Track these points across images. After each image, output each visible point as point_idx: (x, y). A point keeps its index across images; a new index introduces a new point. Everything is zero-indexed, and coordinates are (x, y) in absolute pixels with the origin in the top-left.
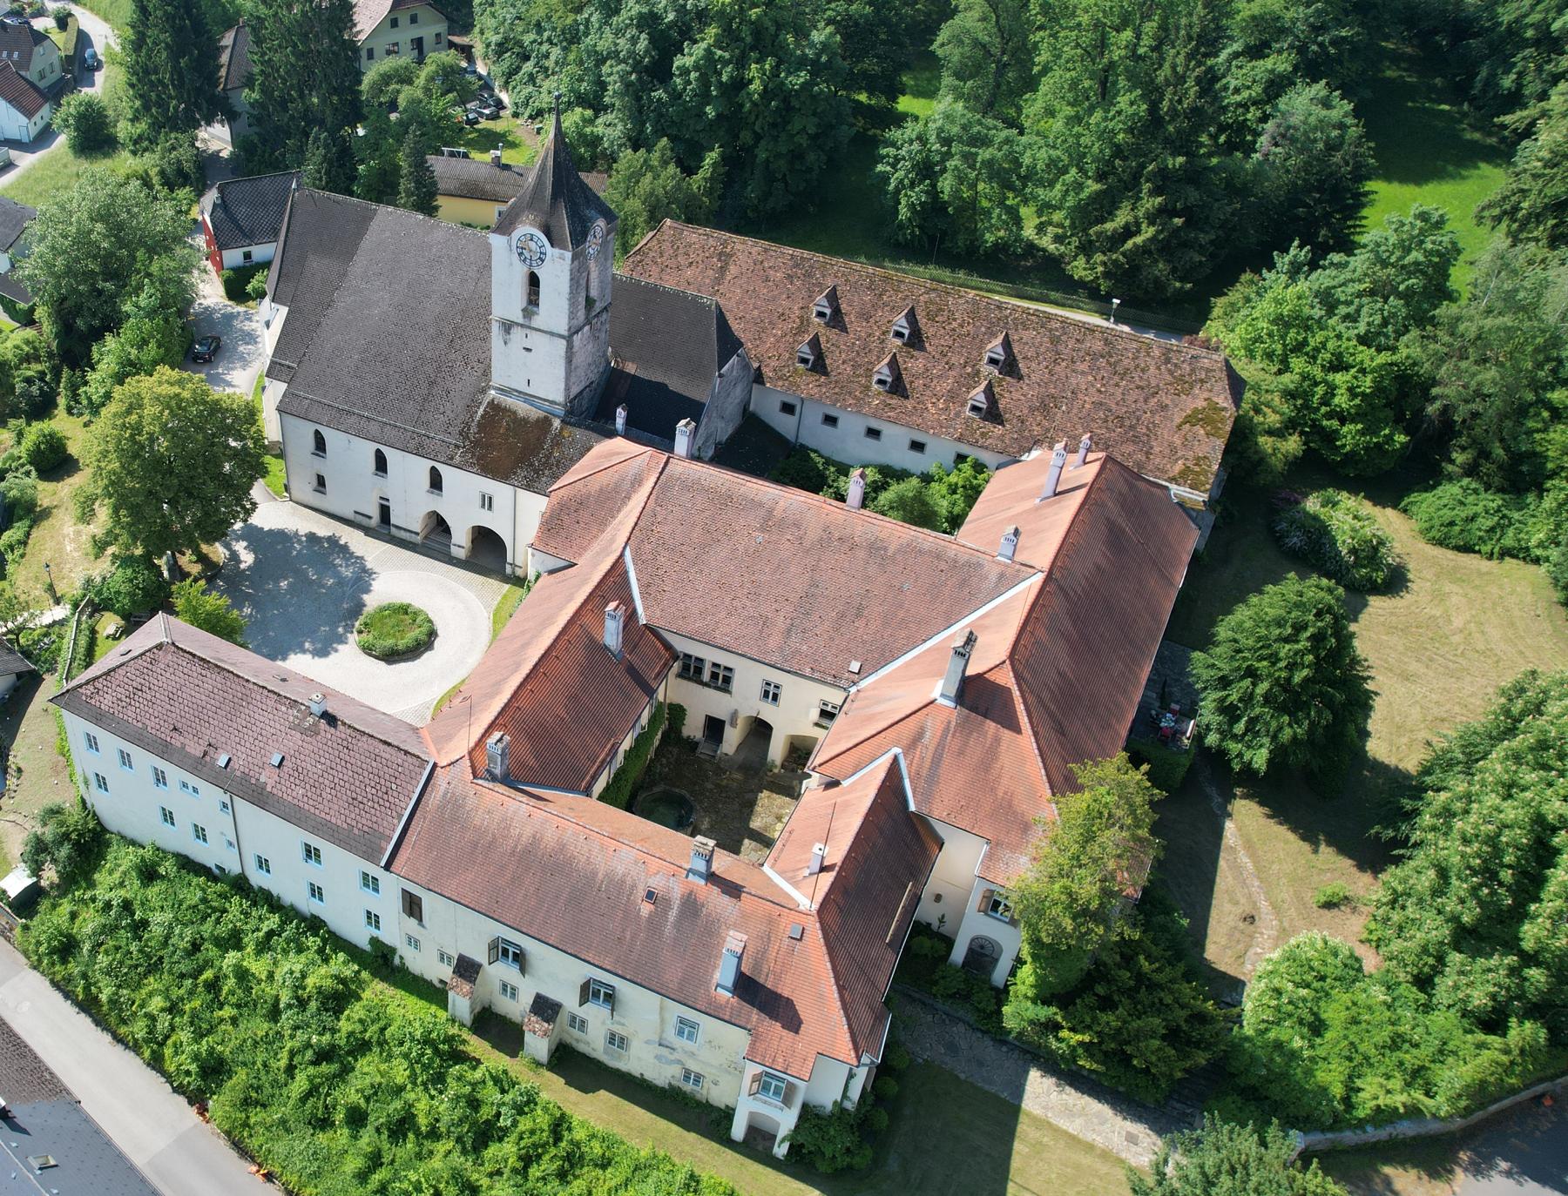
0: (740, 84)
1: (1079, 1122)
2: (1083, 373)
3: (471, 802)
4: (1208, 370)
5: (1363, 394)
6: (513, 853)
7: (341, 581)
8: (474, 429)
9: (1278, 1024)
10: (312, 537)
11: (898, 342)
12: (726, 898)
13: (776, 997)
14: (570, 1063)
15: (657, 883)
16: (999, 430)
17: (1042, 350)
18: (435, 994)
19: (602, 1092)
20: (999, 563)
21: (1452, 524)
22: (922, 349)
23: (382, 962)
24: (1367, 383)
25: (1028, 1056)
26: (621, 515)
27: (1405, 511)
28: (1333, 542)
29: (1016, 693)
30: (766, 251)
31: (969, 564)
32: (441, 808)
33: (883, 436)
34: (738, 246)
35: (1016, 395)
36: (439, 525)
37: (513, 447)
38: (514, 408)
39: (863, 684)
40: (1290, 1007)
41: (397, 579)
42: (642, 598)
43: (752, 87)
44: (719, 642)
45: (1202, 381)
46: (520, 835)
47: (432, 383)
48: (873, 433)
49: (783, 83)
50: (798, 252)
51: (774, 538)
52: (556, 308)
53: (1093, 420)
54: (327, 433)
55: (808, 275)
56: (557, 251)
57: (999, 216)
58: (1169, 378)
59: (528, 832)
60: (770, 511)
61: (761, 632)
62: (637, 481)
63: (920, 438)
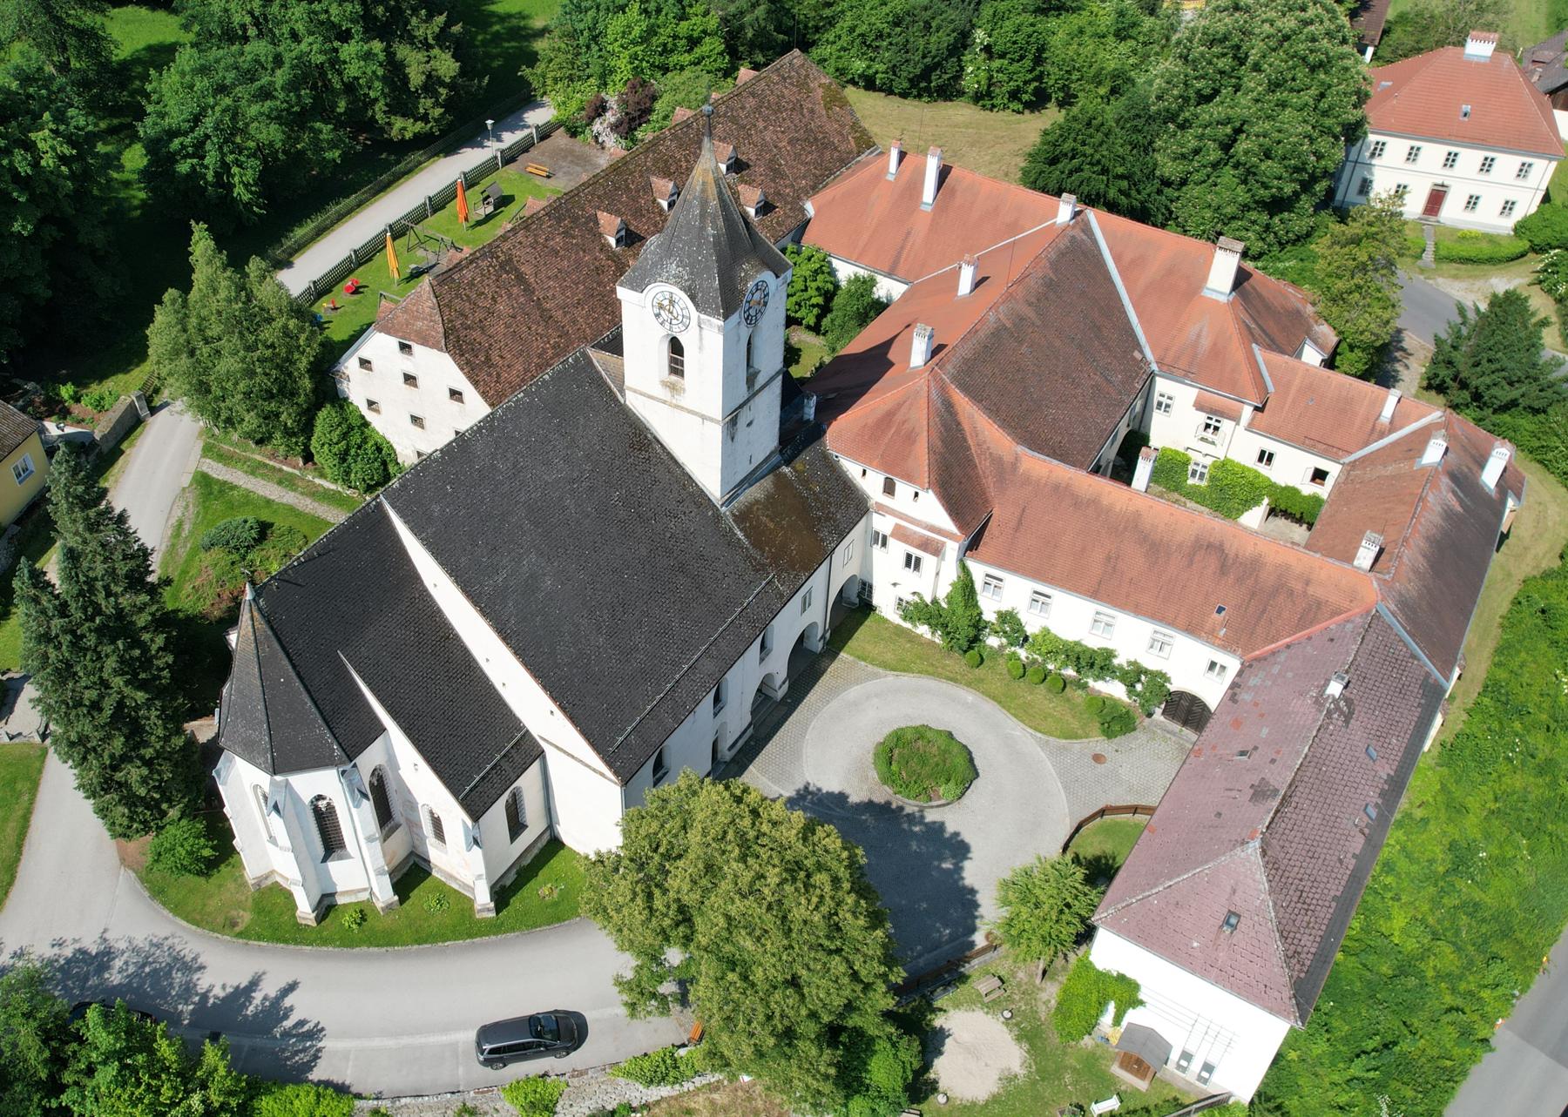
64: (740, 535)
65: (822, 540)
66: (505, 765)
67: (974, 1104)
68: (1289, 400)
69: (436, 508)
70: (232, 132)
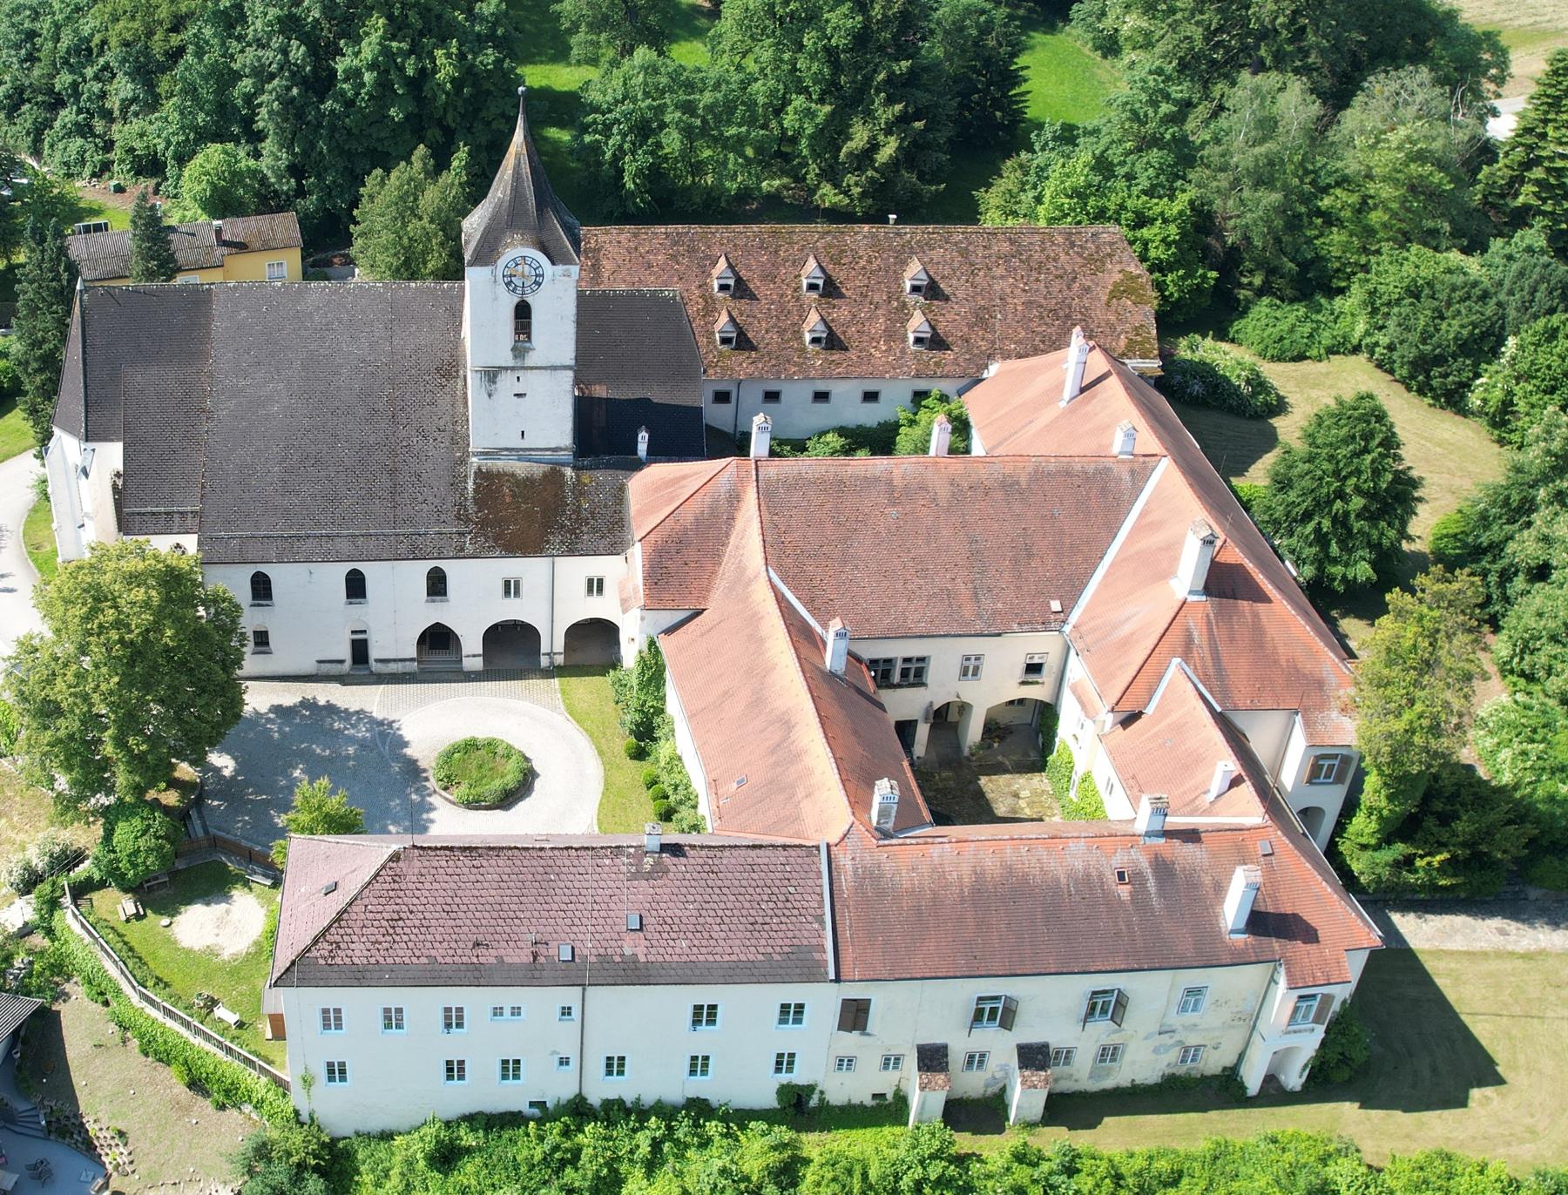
0: (424, 75)
1: (1459, 937)
2: (1002, 277)
3: (887, 867)
4: (1111, 244)
5: (1174, 241)
6: (963, 900)
7: (363, 745)
8: (472, 508)
9: (1538, 781)
10: (277, 709)
11: (814, 295)
12: (1190, 845)
13: (1283, 917)
14: (1068, 1109)
15: (1119, 860)
16: (950, 356)
17: (956, 265)
18: (890, 1110)
19: (1106, 1119)
20: (1123, 461)
21: (1281, 339)
22: (841, 296)
23: (799, 1108)
24: (1173, 231)
25: (1380, 905)
26: (732, 540)
27: (1233, 341)
28: (1226, 380)
29: (1250, 566)
30: (635, 235)
31: (1098, 472)
32: (859, 887)
33: (833, 398)
34: (602, 238)
35: (949, 317)
36: (438, 639)
37: (530, 514)
38: (509, 469)
39: (1074, 617)
40: (1540, 762)
41: (430, 720)
42: (813, 615)
43: (440, 76)
44: (917, 631)
45: (1109, 255)
46: (960, 878)
47: (393, 472)
48: (822, 396)
49: (473, 65)
50: (671, 228)
51: (908, 508)
52: (556, 333)
53: (1031, 320)
54: (272, 571)
55: (692, 250)
56: (560, 268)
57: (736, 163)
58: (1079, 260)
59: (966, 870)
60: (890, 483)
61: (950, 605)
62: (735, 499)
63: (871, 386)
64: (470, 485)
65: (548, 542)
66: (176, 517)
67: (175, 942)
68: (1156, 730)
69: (244, 314)
70: (644, 130)
